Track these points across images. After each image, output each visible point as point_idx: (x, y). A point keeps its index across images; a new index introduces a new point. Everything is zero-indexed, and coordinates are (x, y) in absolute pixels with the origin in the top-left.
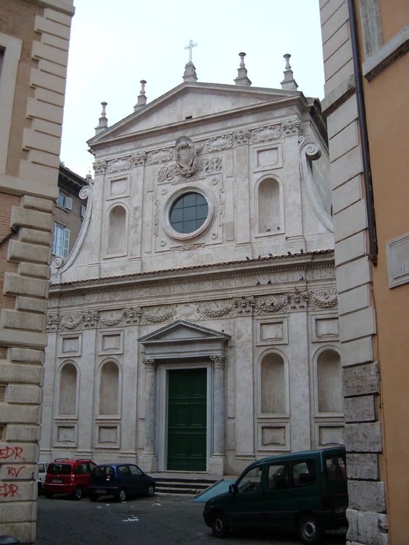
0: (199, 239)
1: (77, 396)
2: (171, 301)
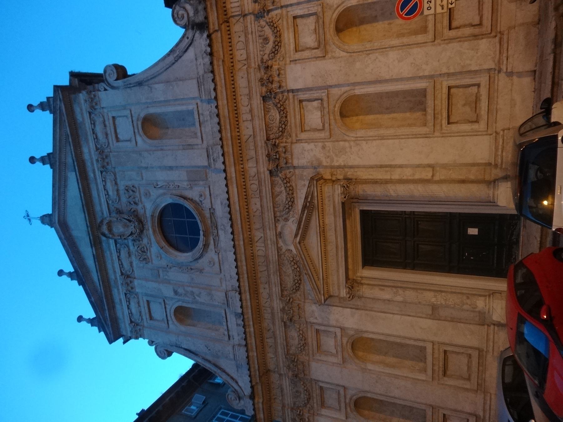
1: (398, 402)
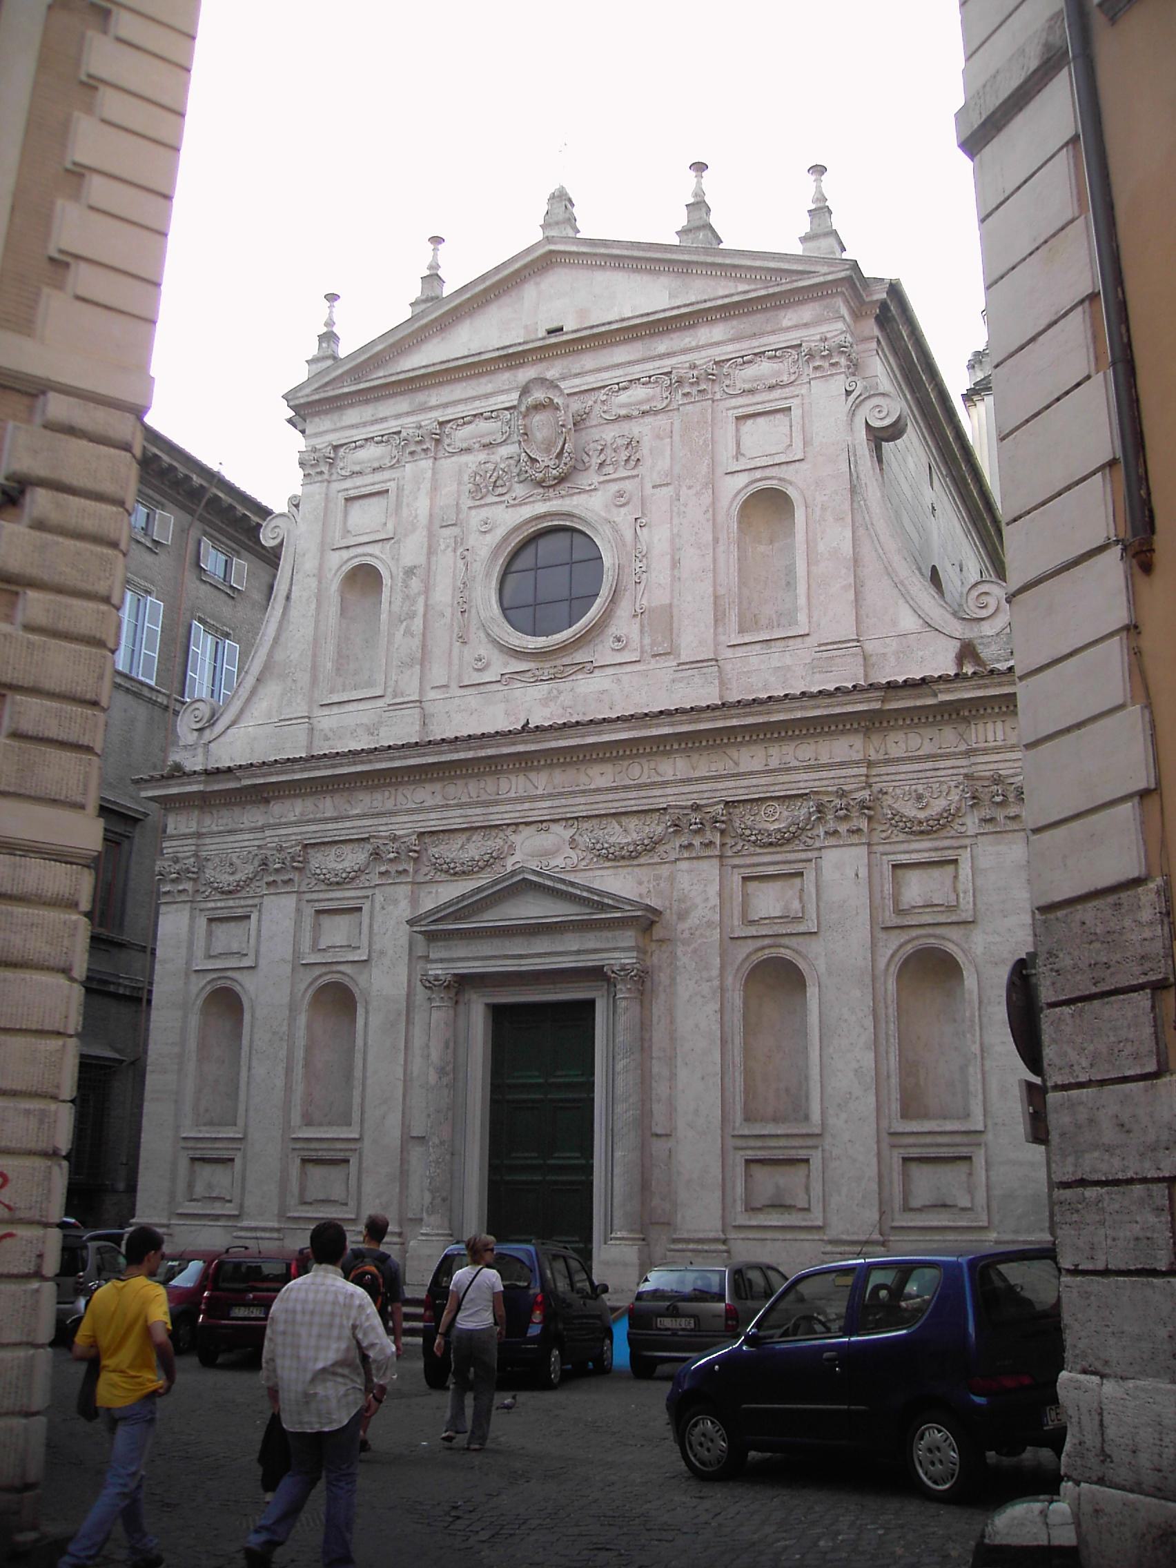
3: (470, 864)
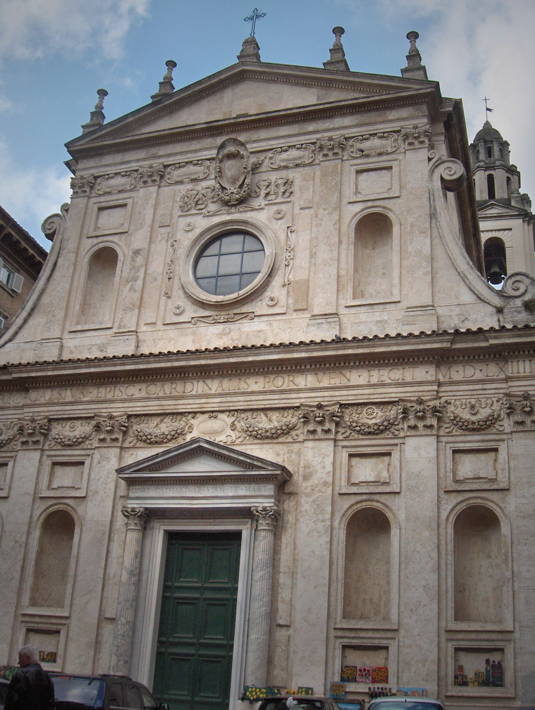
0: (243, 305)
2: (184, 407)
3: (161, 436)
